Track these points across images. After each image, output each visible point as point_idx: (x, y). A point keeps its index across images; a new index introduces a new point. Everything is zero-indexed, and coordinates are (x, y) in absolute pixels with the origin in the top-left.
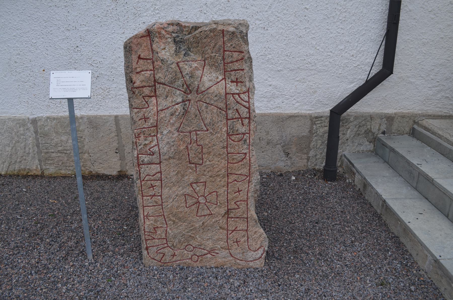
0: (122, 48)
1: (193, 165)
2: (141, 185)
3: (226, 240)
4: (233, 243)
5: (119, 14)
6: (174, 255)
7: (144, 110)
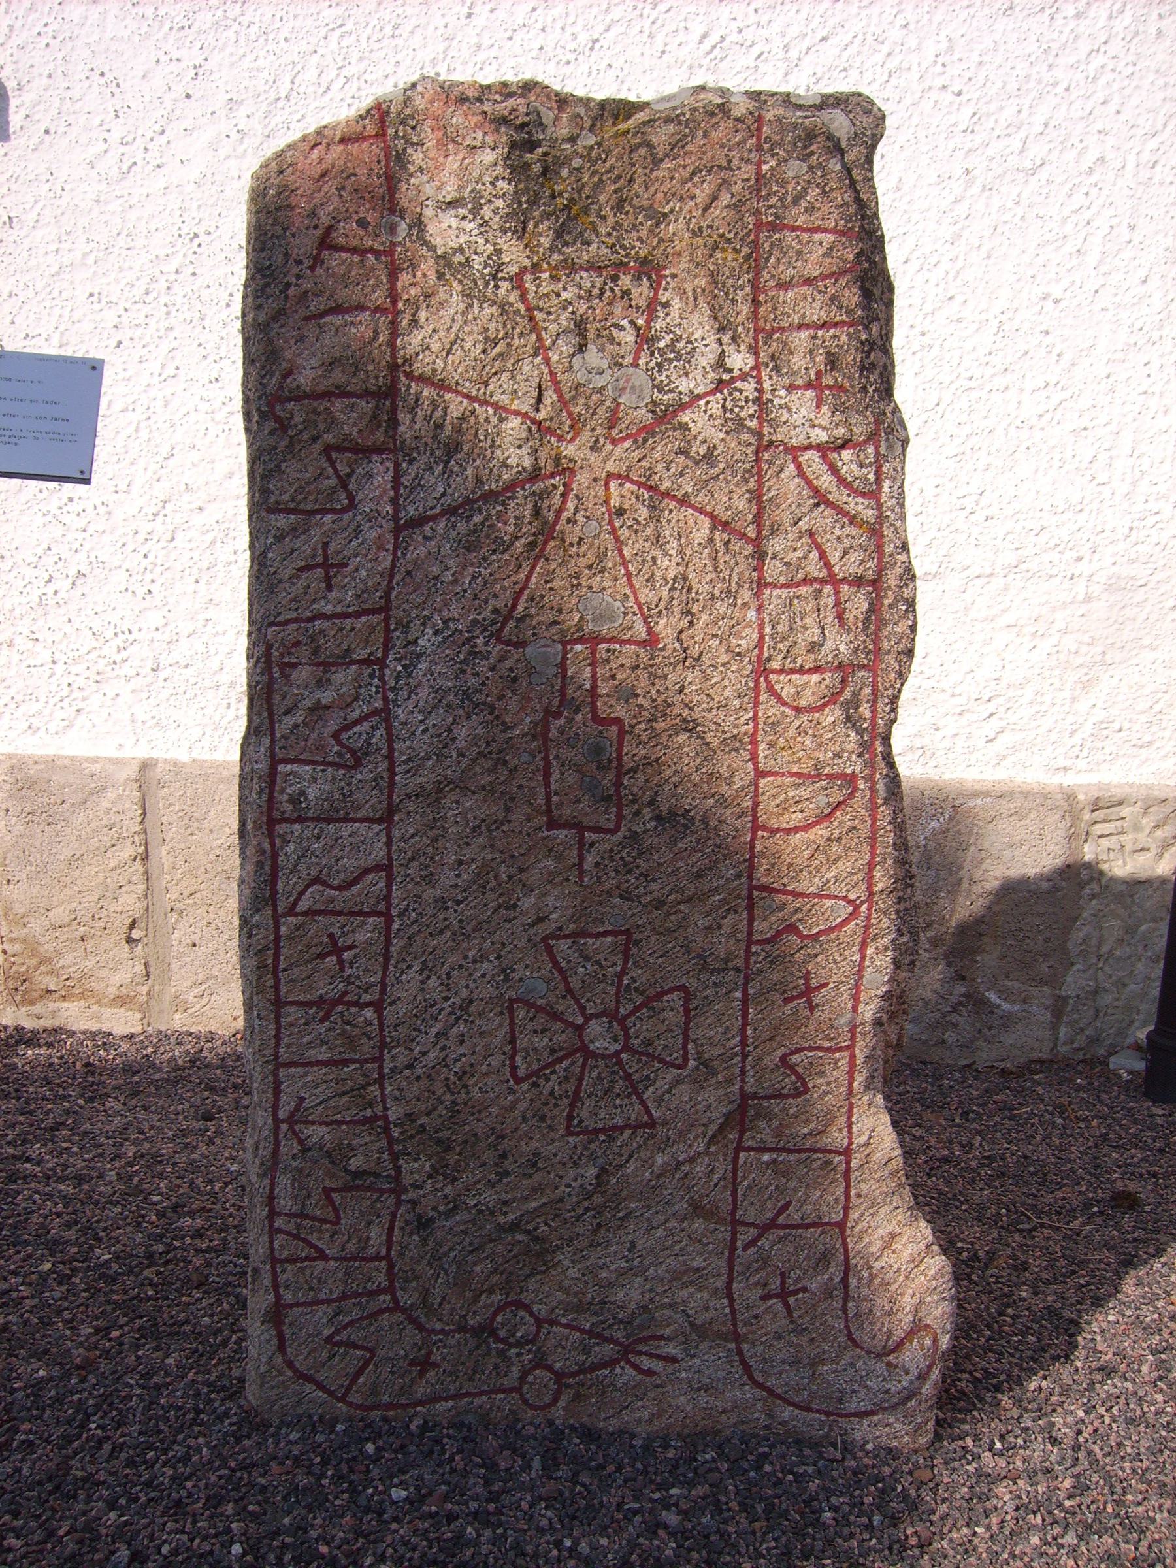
1: (562, 834)
3: (720, 1283)
4: (764, 1298)
5: (205, 294)
6: (424, 1364)
7: (329, 517)
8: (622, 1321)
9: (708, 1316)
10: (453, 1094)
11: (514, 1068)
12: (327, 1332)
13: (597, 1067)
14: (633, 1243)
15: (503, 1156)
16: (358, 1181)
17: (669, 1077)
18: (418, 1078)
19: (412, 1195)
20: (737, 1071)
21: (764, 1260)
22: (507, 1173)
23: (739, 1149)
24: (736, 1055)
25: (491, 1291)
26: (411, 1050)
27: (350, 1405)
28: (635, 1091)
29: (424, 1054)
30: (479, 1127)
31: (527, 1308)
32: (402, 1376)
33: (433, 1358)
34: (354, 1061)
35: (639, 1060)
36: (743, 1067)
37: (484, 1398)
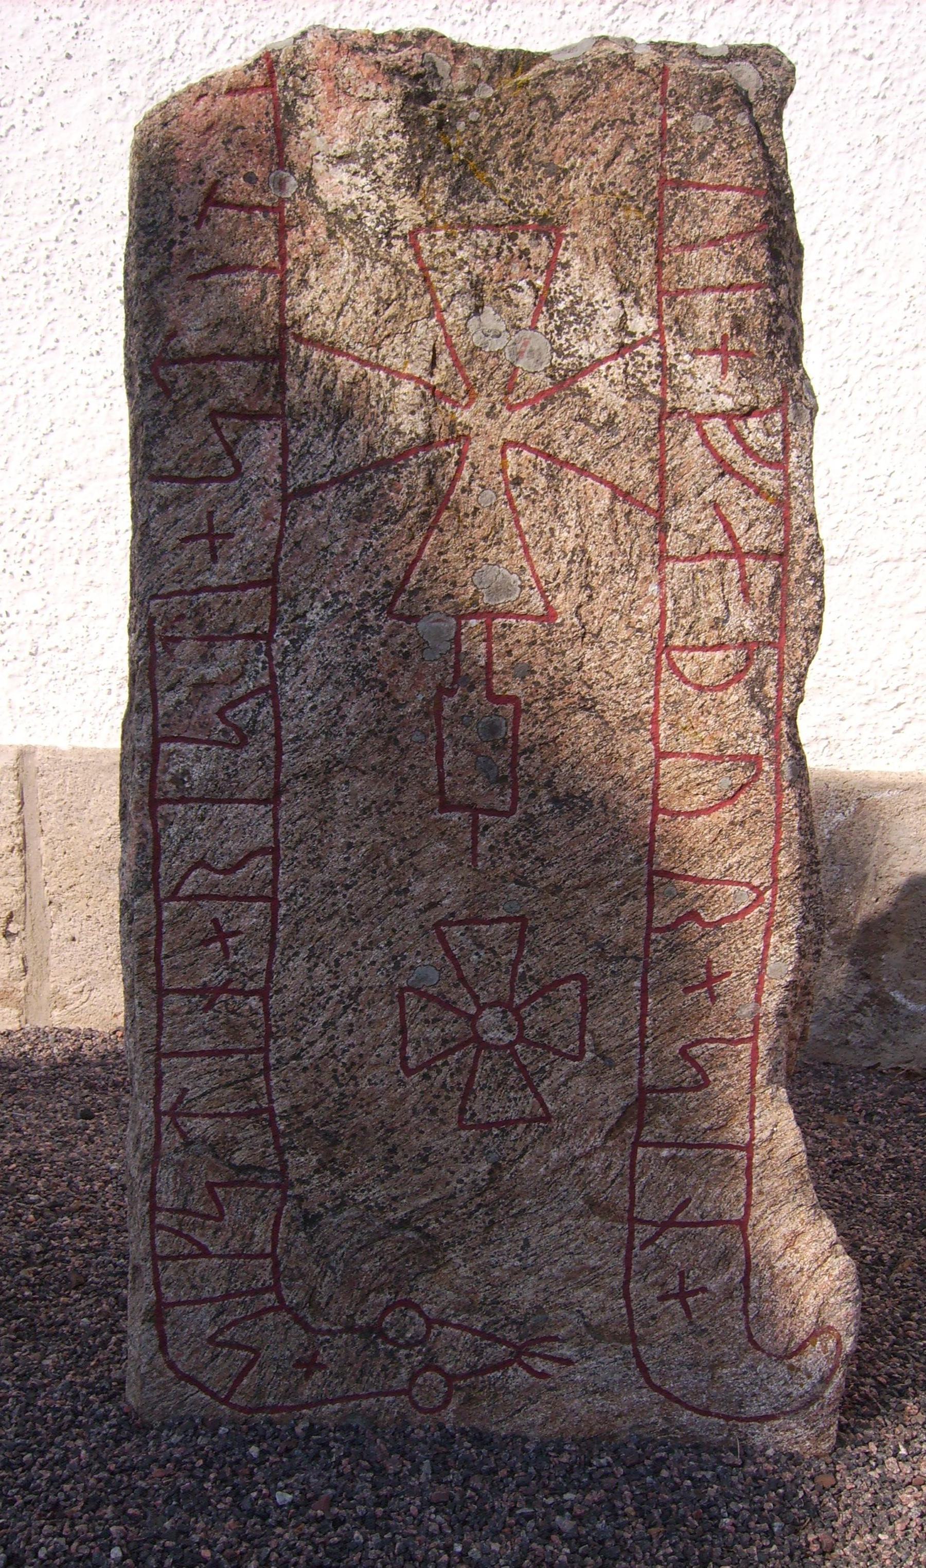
0: (822, 402)
1: (455, 816)
2: (160, 923)
3: (617, 1283)
4: (662, 1298)
10: (341, 1085)
11: (404, 1059)
12: (209, 1332)
15: (393, 1151)
17: (565, 1069)
18: (305, 1069)
19: (298, 1190)
20: (636, 1063)
21: (663, 1259)
22: (397, 1168)
23: (636, 1144)
25: (379, 1290)
26: (298, 1040)
27: (233, 1407)
28: (530, 1084)
29: (311, 1044)
30: (368, 1121)
33: (319, 1359)
34: (239, 1051)
35: (535, 1052)
37: (373, 1400)
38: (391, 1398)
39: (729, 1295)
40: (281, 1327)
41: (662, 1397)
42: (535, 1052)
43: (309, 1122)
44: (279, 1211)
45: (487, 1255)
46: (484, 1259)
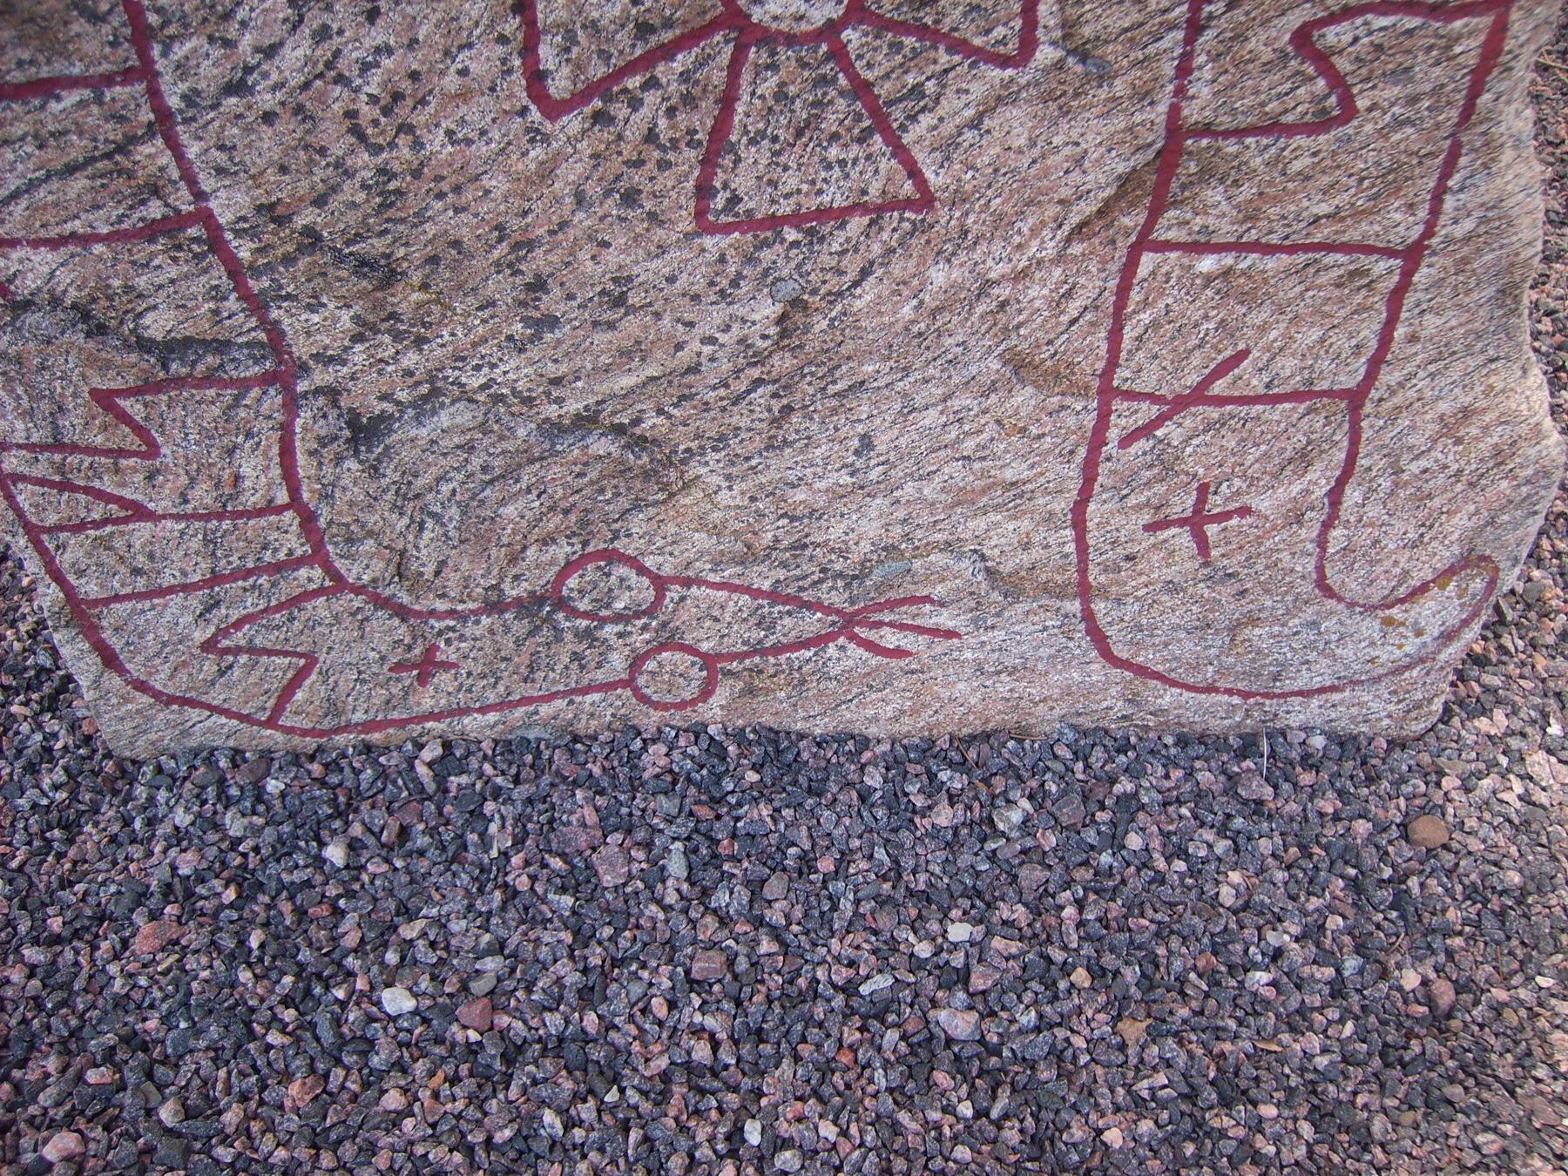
3: (1062, 505)
6: (427, 667)
8: (840, 575)
9: (1025, 558)
10: (376, 150)
11: (536, 79)
12: (200, 636)
13: (773, 67)
14: (867, 443)
15: (538, 285)
16: (174, 362)
17: (977, 90)
18: (268, 118)
19: (322, 376)
20: (1168, 68)
21: (1167, 464)
22: (552, 322)
23: (1144, 243)
24: (1172, 27)
25: (547, 541)
26: (228, 44)
27: (290, 730)
28: (881, 124)
29: (270, 51)
30: (464, 228)
31: (632, 562)
32: (385, 684)
33: (440, 657)
34: (73, 83)
35: (896, 47)
36: (1187, 57)
37: (560, 703)
38: (596, 697)
39: (1297, 518)
40: (347, 620)
41: (1128, 675)
42: (896, 47)
43: (312, 239)
44: (286, 430)
45: (778, 467)
46: (772, 475)
